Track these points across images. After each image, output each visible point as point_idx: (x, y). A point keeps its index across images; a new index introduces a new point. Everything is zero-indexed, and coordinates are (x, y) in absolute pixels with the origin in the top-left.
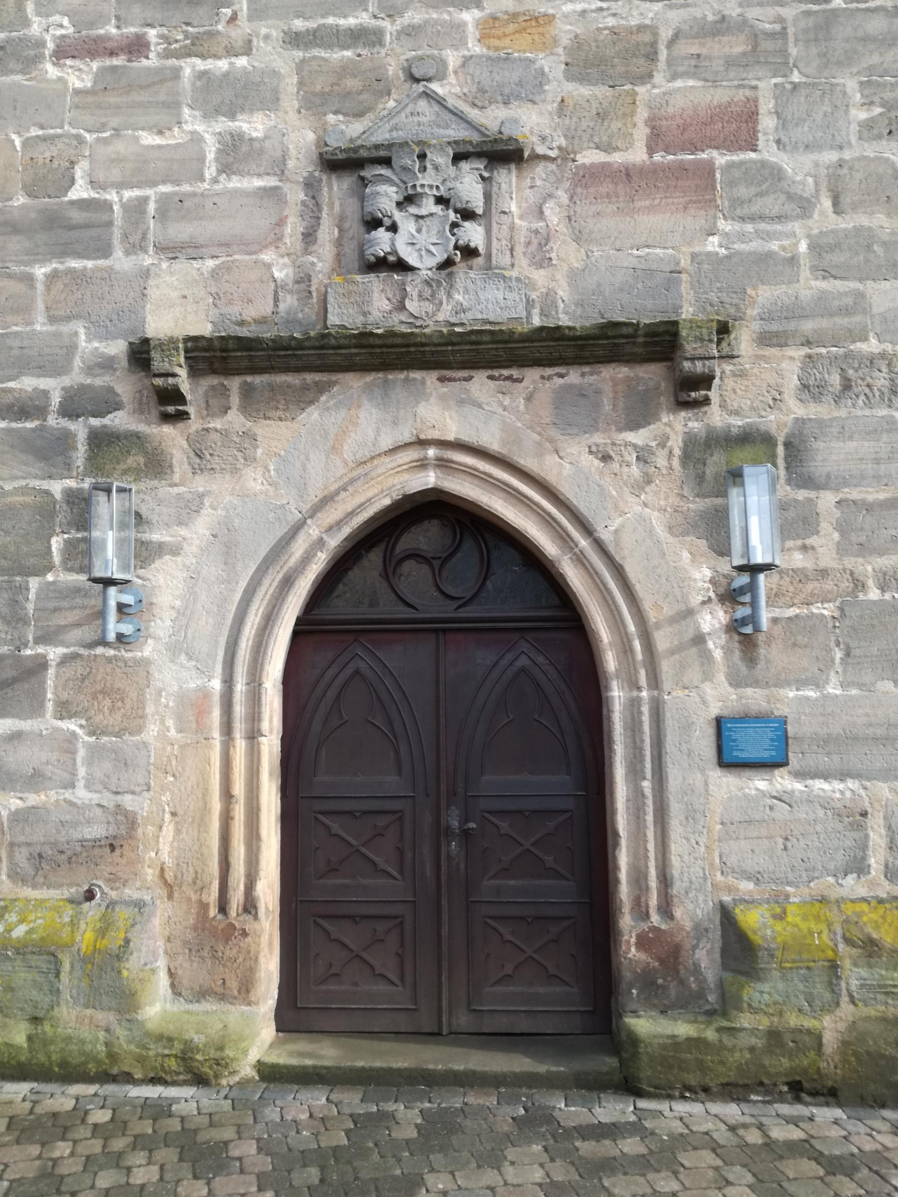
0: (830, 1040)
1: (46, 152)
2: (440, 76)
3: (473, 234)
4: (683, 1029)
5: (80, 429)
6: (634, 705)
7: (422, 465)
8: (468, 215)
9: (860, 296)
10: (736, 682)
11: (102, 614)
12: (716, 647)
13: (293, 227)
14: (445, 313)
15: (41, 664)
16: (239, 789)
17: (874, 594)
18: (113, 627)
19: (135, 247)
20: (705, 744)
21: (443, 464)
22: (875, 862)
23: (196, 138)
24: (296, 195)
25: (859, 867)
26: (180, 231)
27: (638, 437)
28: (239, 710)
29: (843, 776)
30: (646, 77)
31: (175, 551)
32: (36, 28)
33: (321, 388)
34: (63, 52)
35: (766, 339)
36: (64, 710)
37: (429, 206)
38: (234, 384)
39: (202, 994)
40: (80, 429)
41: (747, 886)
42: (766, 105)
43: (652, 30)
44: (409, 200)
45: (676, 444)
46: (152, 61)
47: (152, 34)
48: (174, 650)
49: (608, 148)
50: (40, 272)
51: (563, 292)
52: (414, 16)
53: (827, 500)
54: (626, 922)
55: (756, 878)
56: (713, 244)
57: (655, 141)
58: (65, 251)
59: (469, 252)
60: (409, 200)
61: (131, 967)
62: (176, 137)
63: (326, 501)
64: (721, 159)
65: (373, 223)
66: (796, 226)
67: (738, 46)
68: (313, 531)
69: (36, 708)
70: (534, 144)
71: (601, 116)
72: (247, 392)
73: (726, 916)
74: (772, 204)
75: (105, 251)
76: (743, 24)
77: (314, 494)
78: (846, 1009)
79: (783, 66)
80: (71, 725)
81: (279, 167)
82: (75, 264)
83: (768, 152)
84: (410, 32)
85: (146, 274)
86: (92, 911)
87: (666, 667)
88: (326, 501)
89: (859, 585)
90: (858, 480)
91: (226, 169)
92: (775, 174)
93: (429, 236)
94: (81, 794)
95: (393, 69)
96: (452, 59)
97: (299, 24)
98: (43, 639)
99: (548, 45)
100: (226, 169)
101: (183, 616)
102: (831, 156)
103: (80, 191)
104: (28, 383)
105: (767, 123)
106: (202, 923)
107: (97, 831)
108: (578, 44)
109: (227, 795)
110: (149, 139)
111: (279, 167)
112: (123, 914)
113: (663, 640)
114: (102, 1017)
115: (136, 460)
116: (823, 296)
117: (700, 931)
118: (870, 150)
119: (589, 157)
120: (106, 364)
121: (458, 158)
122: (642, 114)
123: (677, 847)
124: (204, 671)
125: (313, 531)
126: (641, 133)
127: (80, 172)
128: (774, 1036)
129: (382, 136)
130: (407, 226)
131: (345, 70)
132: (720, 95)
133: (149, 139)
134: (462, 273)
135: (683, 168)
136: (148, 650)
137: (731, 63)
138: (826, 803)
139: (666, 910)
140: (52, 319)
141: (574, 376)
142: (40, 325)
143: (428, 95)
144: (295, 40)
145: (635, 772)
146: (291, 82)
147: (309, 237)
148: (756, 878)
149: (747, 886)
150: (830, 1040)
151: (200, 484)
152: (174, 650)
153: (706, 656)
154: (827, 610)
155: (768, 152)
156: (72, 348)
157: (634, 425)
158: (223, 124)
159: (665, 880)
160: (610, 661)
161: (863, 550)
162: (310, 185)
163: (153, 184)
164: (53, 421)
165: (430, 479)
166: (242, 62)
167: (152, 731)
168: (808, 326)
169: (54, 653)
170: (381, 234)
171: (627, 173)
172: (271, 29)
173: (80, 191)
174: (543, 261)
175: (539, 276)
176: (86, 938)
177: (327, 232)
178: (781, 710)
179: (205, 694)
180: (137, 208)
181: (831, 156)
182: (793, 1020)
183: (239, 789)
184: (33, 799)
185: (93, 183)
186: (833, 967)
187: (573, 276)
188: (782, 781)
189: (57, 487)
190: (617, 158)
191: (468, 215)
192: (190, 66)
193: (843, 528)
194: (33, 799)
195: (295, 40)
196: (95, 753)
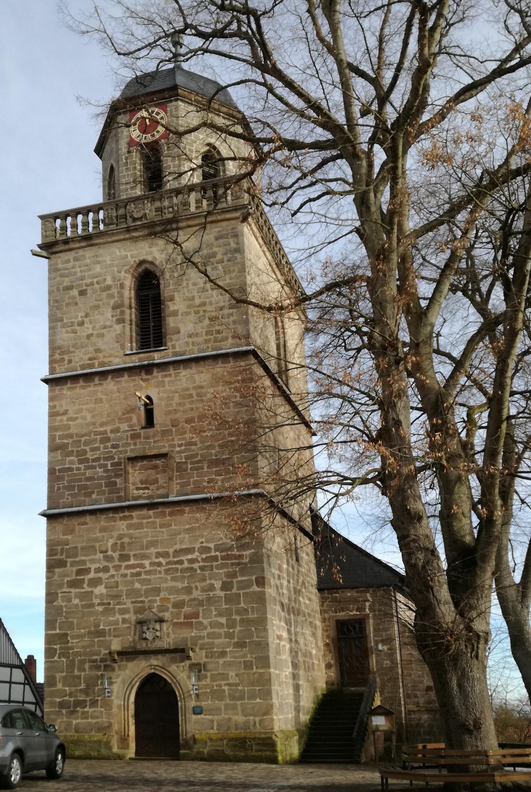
0: (206, 753)
1: (96, 621)
2: (154, 608)
3: (158, 634)
4: (186, 751)
5: (102, 664)
6: (182, 705)
7: (151, 669)
8: (157, 631)
9: (213, 642)
10: (196, 701)
11: (105, 693)
12: (193, 696)
13: (132, 632)
14: (153, 646)
15: (97, 700)
16: (126, 718)
17: (215, 688)
18: (107, 695)
19: (110, 636)
20: (191, 711)
21: (155, 669)
22: (215, 728)
23: (118, 619)
24: (133, 627)
25: (213, 728)
26: (116, 633)
27: (182, 664)
28: (126, 707)
29: (210, 715)
30: (183, 608)
31: (116, 683)
32: (94, 601)
33: (137, 657)
34: (99, 605)
35: (201, 649)
36: (101, 707)
37: (151, 630)
38: (124, 657)
39: (122, 748)
40: (102, 664)
41: (197, 732)
42: (201, 612)
43: (184, 600)
44: (148, 629)
45: (188, 665)
46: (111, 606)
47: (111, 602)
48: (117, 698)
49: (178, 619)
50: (96, 640)
51: (171, 642)
52: (150, 598)
53: (209, 674)
54: (181, 737)
55: (198, 730)
56: (193, 634)
57: (185, 618)
58: (99, 637)
59: (157, 637)
60: (148, 629)
61: (111, 744)
62: (115, 619)
63: (138, 674)
64: (194, 621)
65: (144, 632)
66: (205, 631)
67: (197, 603)
68: (136, 679)
69: (97, 706)
70: (166, 618)
71: (177, 614)
72: (126, 659)
73: (194, 735)
74: (201, 628)
75: (105, 637)
76: (198, 599)
77: (136, 674)
78: (208, 748)
79: (203, 606)
80: (102, 709)
81: (130, 623)
82: (101, 639)
83: (201, 619)
84: (149, 601)
85: (111, 640)
86: (106, 736)
87: (186, 699)
88: (138, 674)
89: (213, 686)
90: (214, 670)
91: (123, 623)
92: (201, 623)
93: (151, 635)
94: (104, 719)
95: (147, 607)
96: (155, 605)
97: (133, 600)
98: (98, 696)
99: (169, 602)
100: (123, 623)
101: (118, 692)
102: (210, 620)
103: (101, 627)
104: (95, 657)
105: (201, 615)
106: (121, 738)
107: (106, 725)
108: (173, 603)
109: (125, 720)
110: (111, 619)
111: (130, 623)
112: (110, 737)
113: (186, 695)
114: (107, 751)
115: (110, 669)
116: (208, 642)
117: (190, 738)
118: (216, 619)
119: (175, 621)
120: (106, 654)
121: (156, 622)
122: (183, 614)
123: (187, 726)
124: (121, 701)
125: (136, 679)
126: (183, 617)
127: (101, 624)
128: (198, 752)
129: (145, 618)
130: (148, 633)
131: (140, 607)
132: (194, 611)
133: (111, 619)
134: (157, 640)
135: (188, 622)
136: (113, 698)
137: (196, 605)
138: (208, 719)
139: (186, 735)
140: (98, 647)
141: (173, 655)
142: (96, 648)
143: (152, 611)
144: (133, 602)
145: (182, 716)
146: (132, 610)
147: (135, 634)
148: (198, 730)
149: (197, 732)
150: (206, 753)
151: (120, 672)
152: (117, 698)
153: (192, 698)
154: (208, 690)
155: (201, 619)
156: (101, 652)
157: (182, 662)
158: (122, 616)
159: (186, 731)
160: (179, 699)
161: (214, 681)
162: (135, 626)
163: (112, 625)
164: (99, 663)
165: (153, 671)
166: (125, 606)
167: (113, 710)
168: (206, 647)
169: (99, 698)
170: (144, 634)
171: (181, 624)
172: (129, 601)
173: (101, 627)
174: (168, 637)
175: (168, 639)
176: (105, 740)
177: (138, 633)
178: (202, 705)
179: (121, 705)
180: (110, 630)
181: (210, 620)
182: (201, 750)
183: (126, 718)
184: (97, 720)
185: (104, 626)
186: (206, 743)
187: (173, 639)
188: (202, 716)
189: (99, 673)
190: (179, 621)
191: (157, 631)
192: (117, 607)
193: (211, 678)
194: (97, 720)
195: (133, 602)
196: (106, 713)
